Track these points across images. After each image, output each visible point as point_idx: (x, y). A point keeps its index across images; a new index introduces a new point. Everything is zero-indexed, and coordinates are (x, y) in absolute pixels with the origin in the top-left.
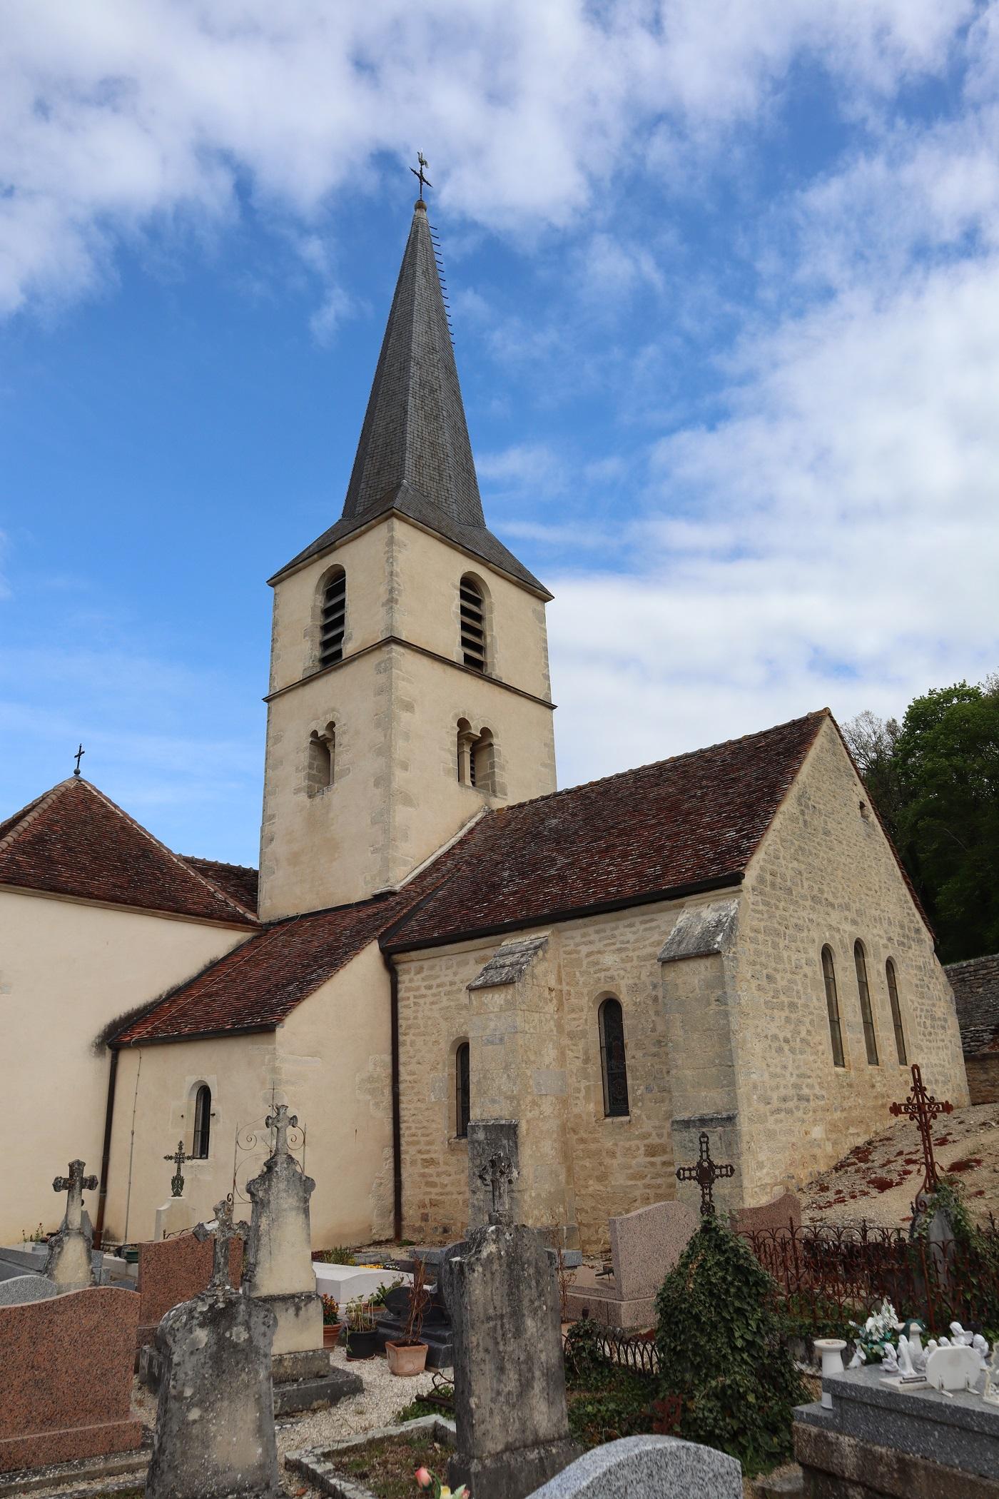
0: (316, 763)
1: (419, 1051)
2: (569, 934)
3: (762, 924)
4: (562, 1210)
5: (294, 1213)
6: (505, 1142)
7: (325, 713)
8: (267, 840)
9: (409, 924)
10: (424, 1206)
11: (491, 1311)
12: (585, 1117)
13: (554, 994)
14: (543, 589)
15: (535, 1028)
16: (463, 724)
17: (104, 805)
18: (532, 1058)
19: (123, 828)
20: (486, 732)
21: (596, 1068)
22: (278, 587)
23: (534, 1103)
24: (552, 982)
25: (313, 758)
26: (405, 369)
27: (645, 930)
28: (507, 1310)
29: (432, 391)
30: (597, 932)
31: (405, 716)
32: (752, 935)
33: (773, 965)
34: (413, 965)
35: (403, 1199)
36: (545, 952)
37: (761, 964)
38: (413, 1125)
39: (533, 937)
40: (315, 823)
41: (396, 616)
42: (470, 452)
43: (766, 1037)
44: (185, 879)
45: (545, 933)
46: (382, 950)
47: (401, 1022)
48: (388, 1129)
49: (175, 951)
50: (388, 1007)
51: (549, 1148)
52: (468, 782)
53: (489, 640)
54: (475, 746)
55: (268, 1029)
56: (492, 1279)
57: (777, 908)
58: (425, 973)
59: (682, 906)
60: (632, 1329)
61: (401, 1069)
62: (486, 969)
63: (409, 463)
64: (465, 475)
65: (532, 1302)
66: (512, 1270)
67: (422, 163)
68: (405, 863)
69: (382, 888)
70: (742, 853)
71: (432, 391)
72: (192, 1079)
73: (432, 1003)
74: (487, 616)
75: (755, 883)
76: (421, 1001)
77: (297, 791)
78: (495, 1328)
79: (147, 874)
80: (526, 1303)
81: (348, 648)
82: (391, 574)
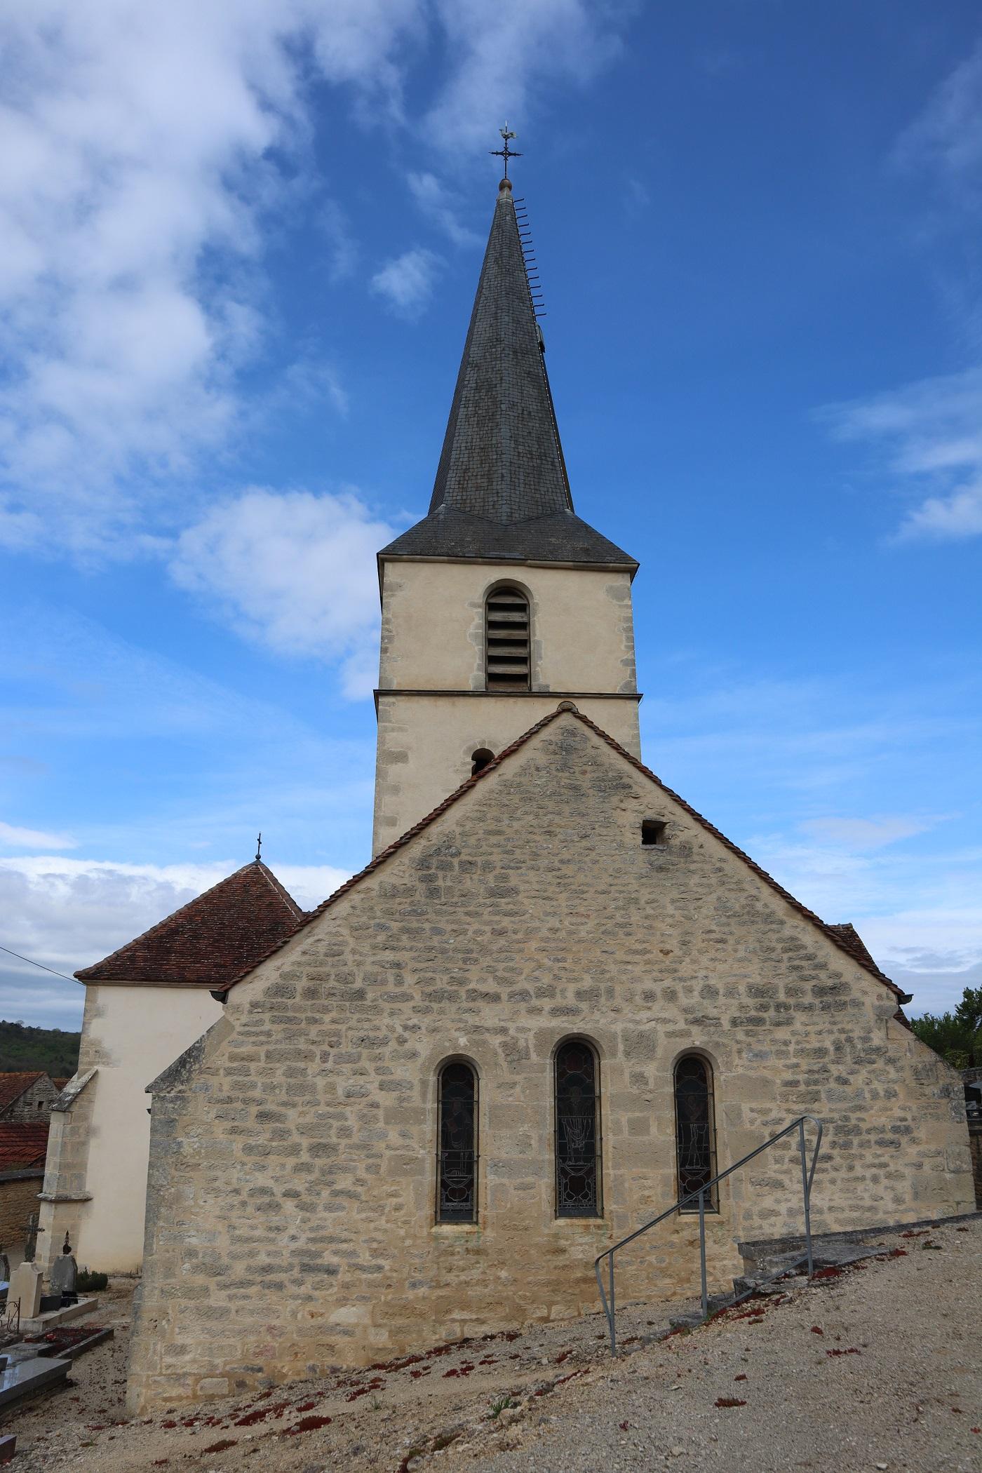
14: (624, 558)
43: (237, 1191)
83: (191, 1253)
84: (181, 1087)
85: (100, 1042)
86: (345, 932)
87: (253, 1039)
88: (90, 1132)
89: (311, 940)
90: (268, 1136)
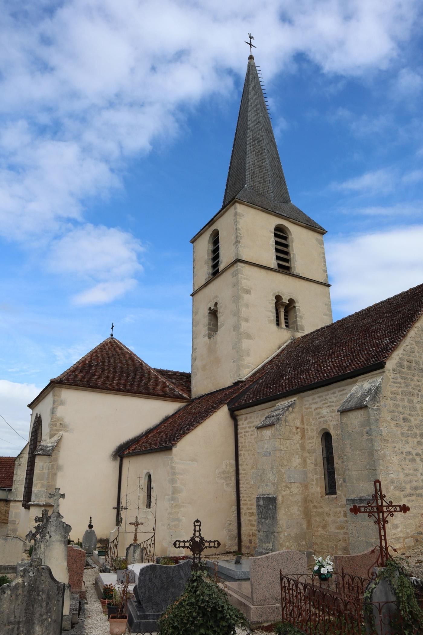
0: (212, 323)
1: (246, 459)
2: (306, 398)
3: (400, 389)
4: (304, 543)
5: (58, 543)
6: (271, 506)
7: (214, 299)
8: (194, 360)
9: (241, 398)
10: (250, 536)
11: (12, 619)
12: (316, 495)
13: (299, 430)
14: (321, 228)
15: (287, 448)
16: (278, 298)
17: (122, 349)
18: (285, 463)
19: (130, 358)
20: (291, 301)
21: (320, 469)
22: (195, 243)
23: (287, 487)
24: (298, 424)
25: (210, 320)
26: (245, 134)
27: (341, 395)
28: (23, 619)
29: (259, 142)
30: (319, 397)
31: (246, 296)
32: (392, 396)
33: (409, 412)
34: (243, 417)
35: (242, 532)
36: (293, 408)
37: (399, 412)
38: (245, 495)
39: (290, 401)
40: (211, 350)
41: (239, 249)
42: (281, 167)
43: (402, 453)
44: (156, 379)
45: (294, 399)
46: (229, 409)
47: (239, 444)
48: (234, 497)
49: (146, 413)
50: (233, 437)
51: (296, 510)
52: (283, 325)
53: (292, 256)
54: (285, 310)
55: (169, 449)
56: (16, 599)
57: (412, 380)
58: (248, 420)
59: (356, 382)
60: (258, 622)
61: (240, 467)
62: (266, 418)
63: (248, 176)
64: (279, 179)
65: (41, 615)
66: (30, 595)
67: (251, 37)
68: (248, 367)
69: (237, 379)
70: (387, 350)
71: (259, 142)
72: (145, 471)
73: (251, 435)
74: (290, 244)
75: (395, 367)
76: (247, 434)
77: (204, 336)
78: (13, 629)
79: (137, 378)
80: (37, 615)
81: (221, 267)
82: (236, 229)
83: (392, 481)
84: (378, 404)
85: (63, 419)
86: (414, 343)
87: (396, 385)
88: (59, 468)
89: (405, 345)
90: (407, 428)
